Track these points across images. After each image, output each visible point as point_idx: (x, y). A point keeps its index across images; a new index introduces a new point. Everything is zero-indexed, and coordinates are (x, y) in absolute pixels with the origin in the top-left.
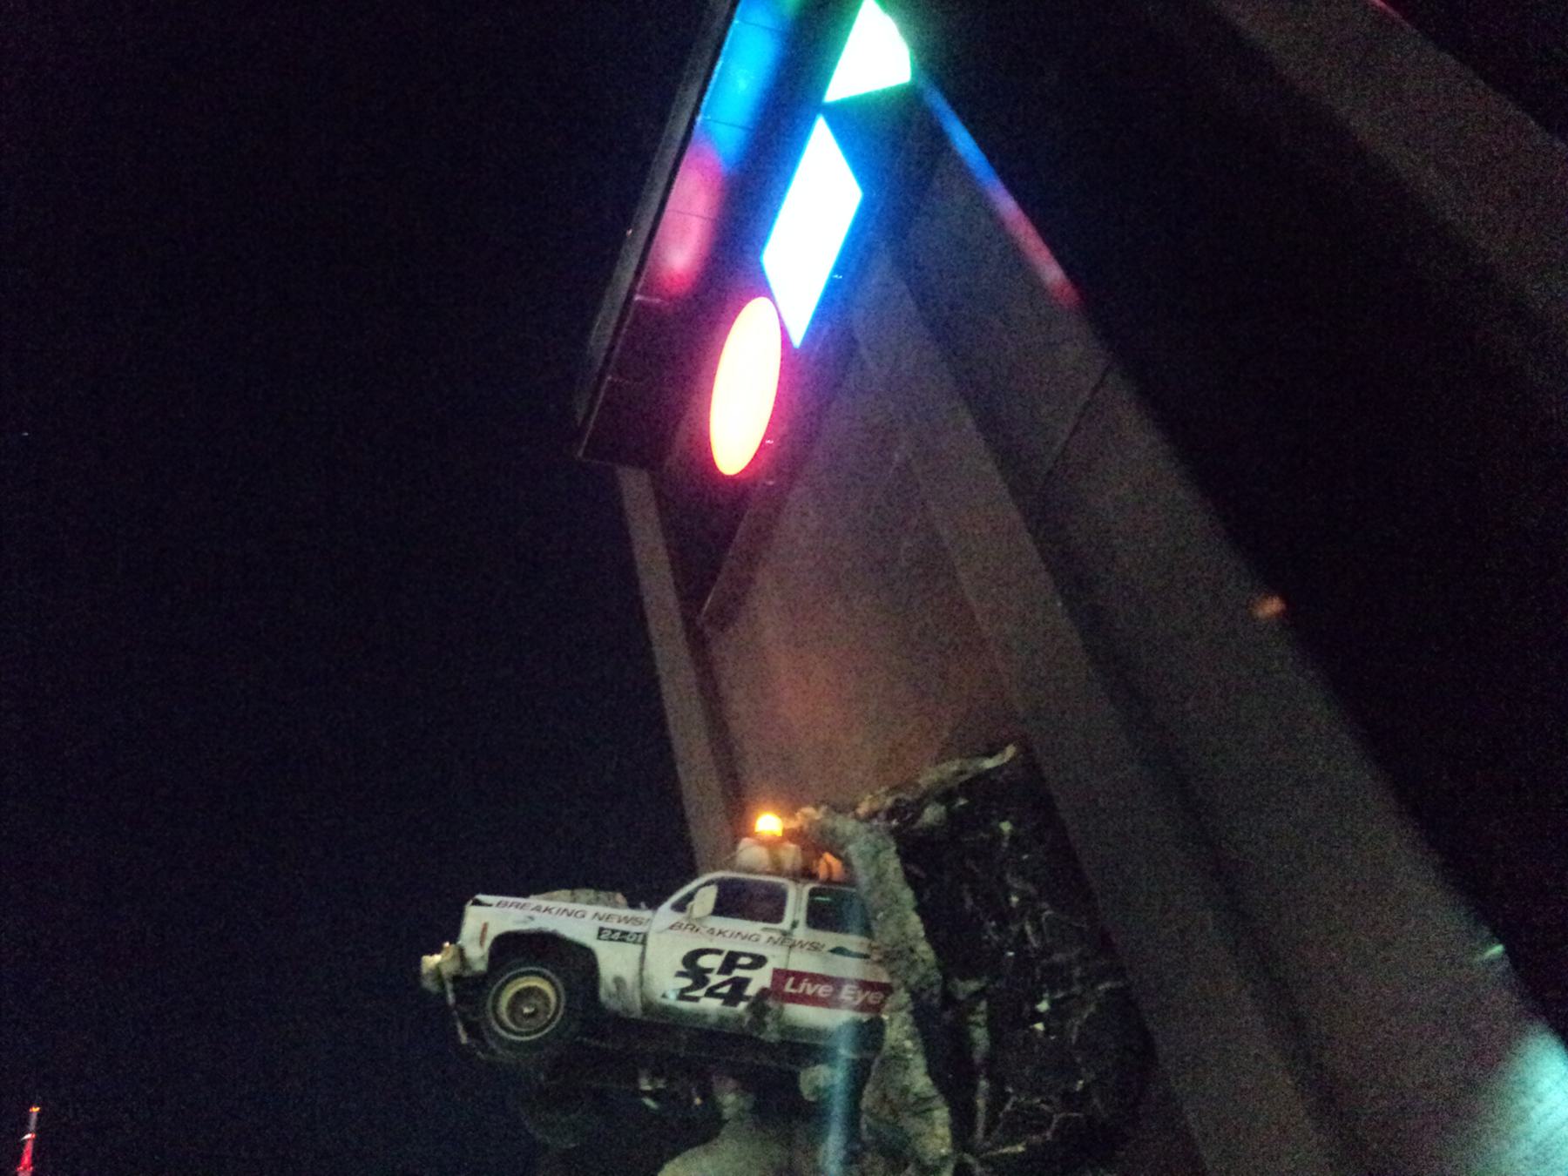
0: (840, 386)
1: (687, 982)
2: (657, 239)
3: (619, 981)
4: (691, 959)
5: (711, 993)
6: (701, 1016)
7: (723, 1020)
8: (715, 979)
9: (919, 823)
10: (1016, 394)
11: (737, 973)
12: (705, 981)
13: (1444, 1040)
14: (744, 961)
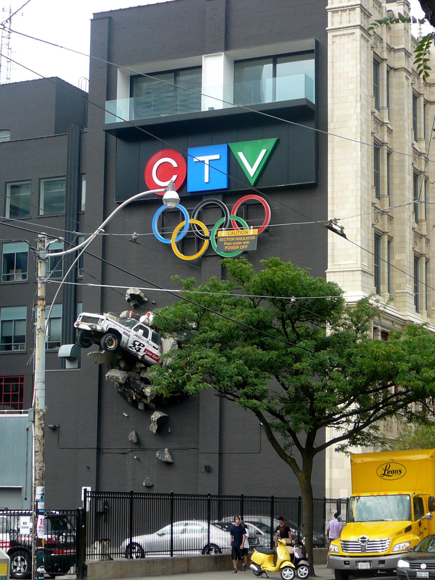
0: (296, 288)
1: (133, 346)
2: (240, 64)
3: (124, 342)
4: (135, 342)
5: (135, 349)
6: (132, 352)
7: (135, 354)
8: (137, 347)
9: (271, 142)
10: (302, 562)
11: (140, 347)
12: (135, 346)
13: (376, 396)
14: (142, 345)
